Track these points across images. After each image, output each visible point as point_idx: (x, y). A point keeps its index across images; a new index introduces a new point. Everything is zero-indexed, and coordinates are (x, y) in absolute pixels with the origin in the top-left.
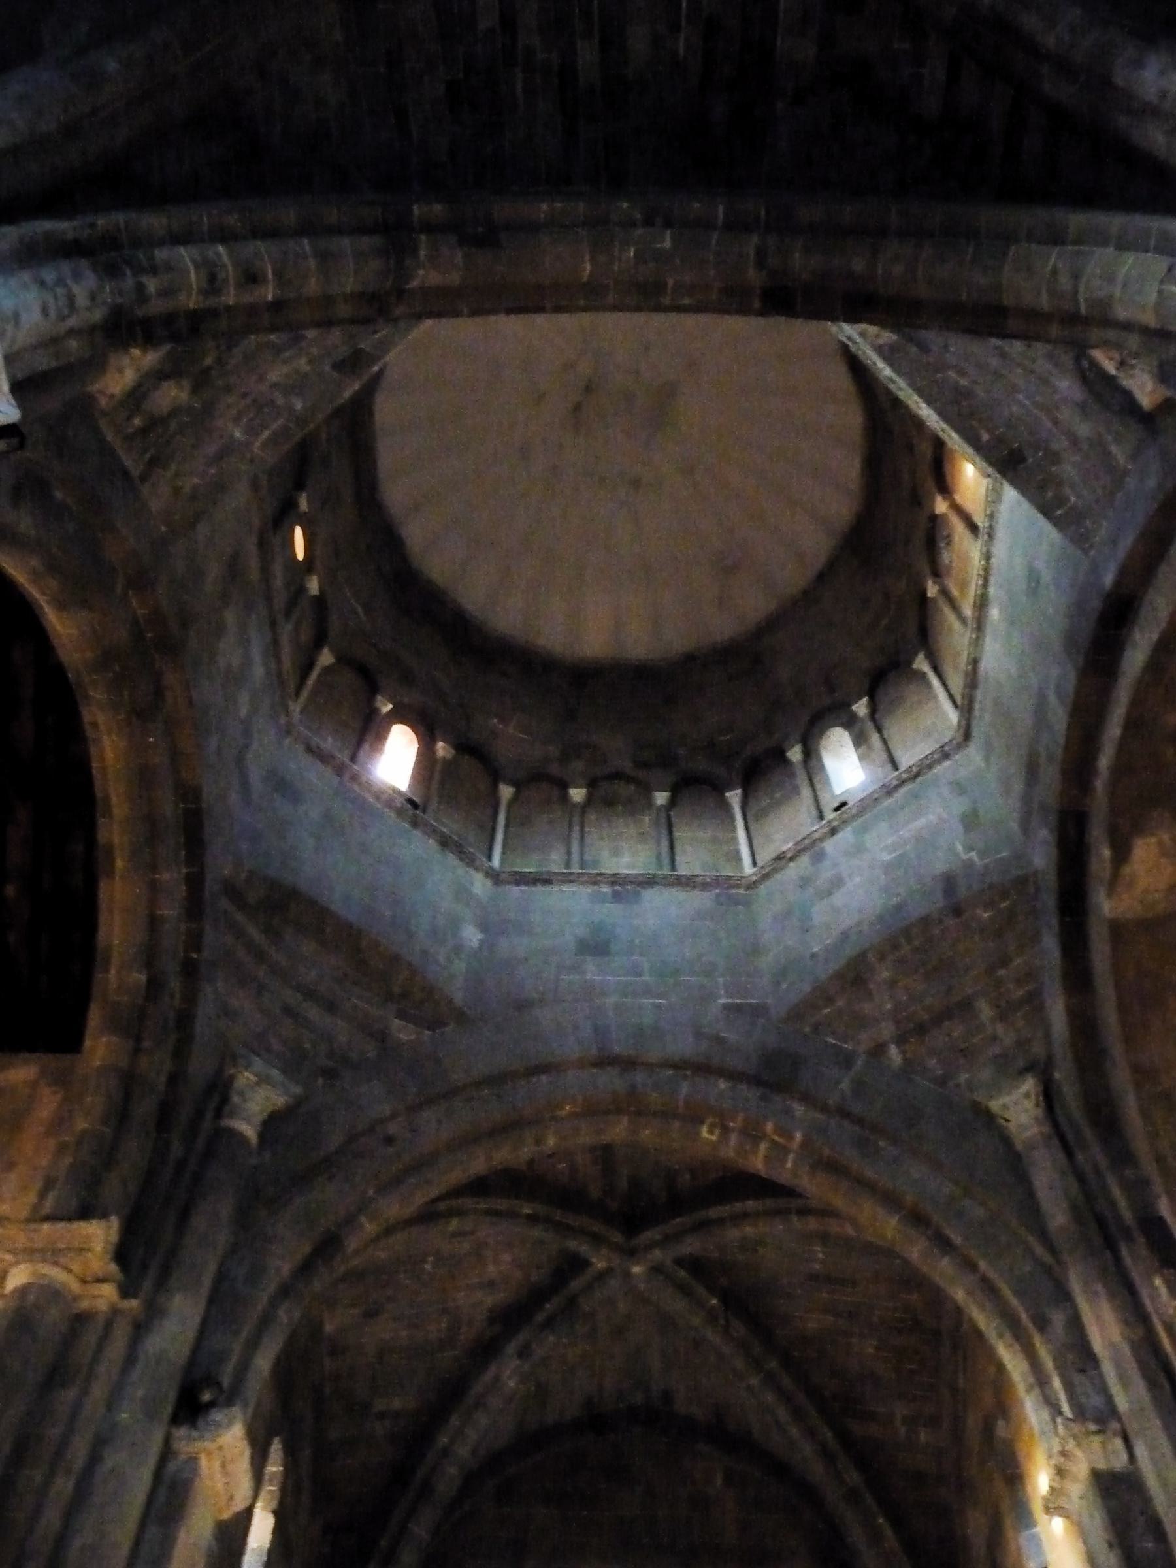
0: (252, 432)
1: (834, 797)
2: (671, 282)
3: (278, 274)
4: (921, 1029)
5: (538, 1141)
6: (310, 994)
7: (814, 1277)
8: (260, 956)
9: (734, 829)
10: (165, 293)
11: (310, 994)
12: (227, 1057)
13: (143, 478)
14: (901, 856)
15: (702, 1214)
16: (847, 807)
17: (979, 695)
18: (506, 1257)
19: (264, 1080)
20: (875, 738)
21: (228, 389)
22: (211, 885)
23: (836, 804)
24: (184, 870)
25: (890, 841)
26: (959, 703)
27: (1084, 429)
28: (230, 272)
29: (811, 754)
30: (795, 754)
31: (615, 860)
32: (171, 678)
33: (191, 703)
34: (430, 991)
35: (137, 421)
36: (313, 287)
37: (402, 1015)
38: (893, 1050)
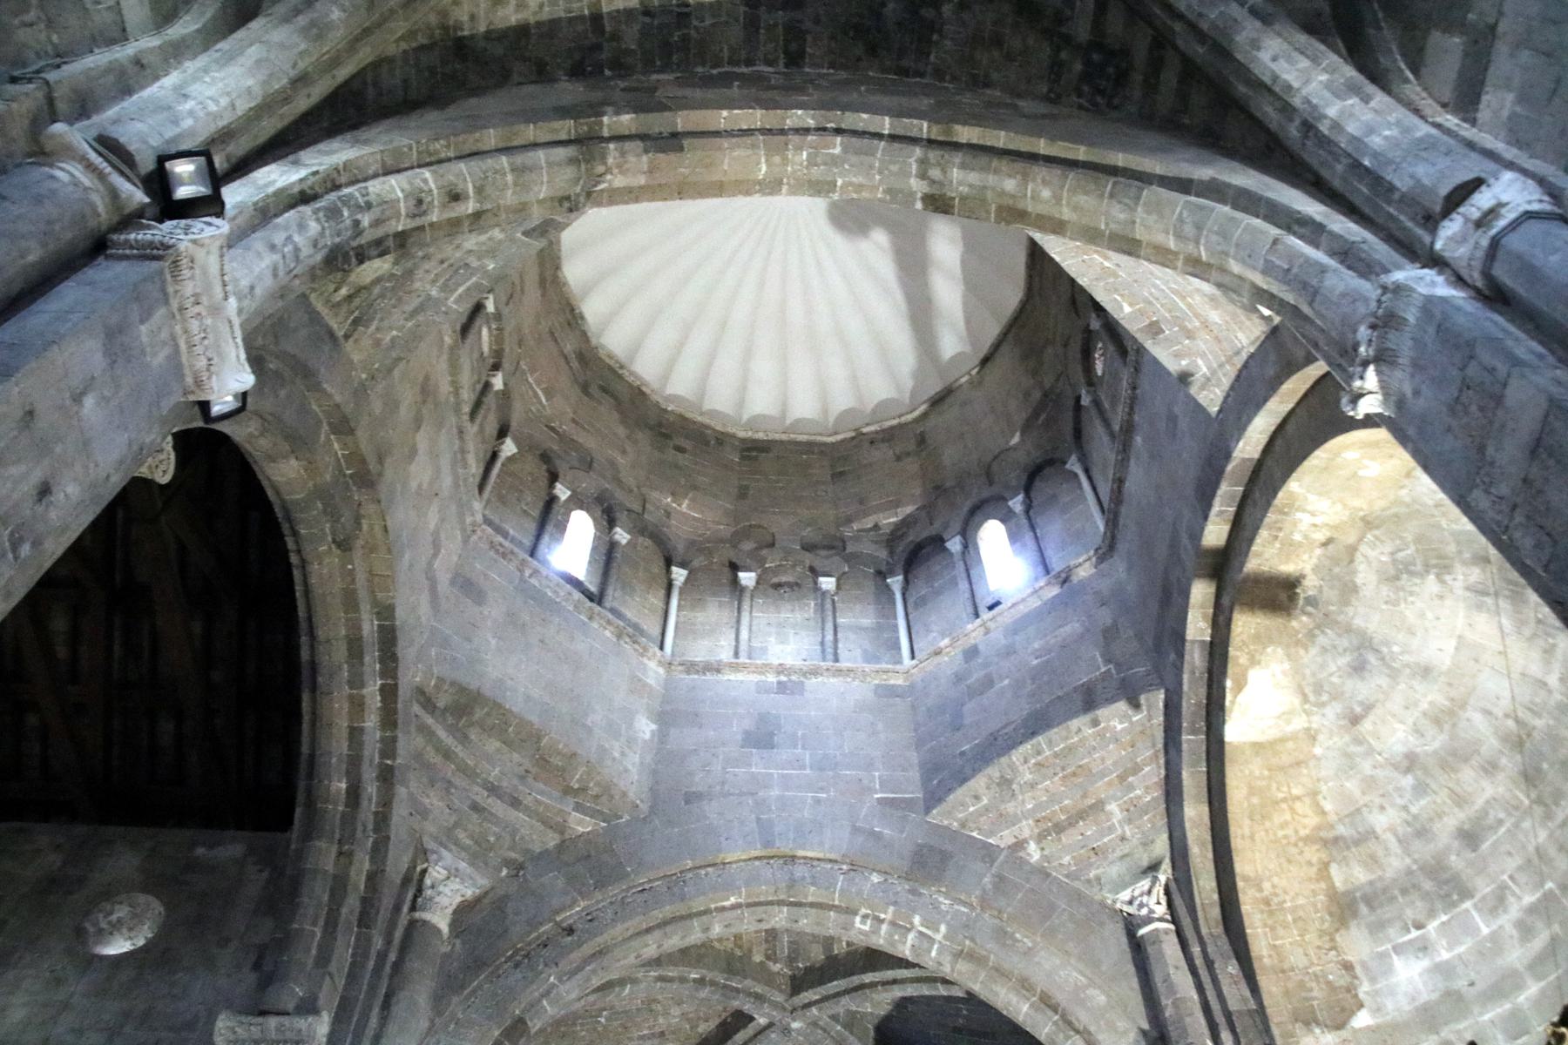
0: (447, 288)
1: (989, 593)
2: (840, 182)
3: (480, 190)
4: (1059, 828)
5: (707, 930)
6: (493, 790)
7: (957, 1030)
8: (448, 755)
9: (895, 617)
10: (376, 223)
11: (493, 790)
12: (422, 853)
13: (347, 337)
14: (1047, 662)
15: (856, 980)
16: (1000, 607)
17: (1123, 510)
18: (675, 1011)
19: (453, 873)
20: (1029, 536)
21: (426, 257)
22: (404, 692)
23: (990, 604)
24: (379, 682)
25: (1036, 645)
26: (1106, 506)
27: (1215, 316)
28: (436, 197)
29: (969, 544)
30: (954, 545)
31: (781, 647)
32: (370, 509)
33: (385, 529)
34: (607, 789)
35: (344, 291)
36: (510, 198)
37: (578, 808)
38: (1032, 847)
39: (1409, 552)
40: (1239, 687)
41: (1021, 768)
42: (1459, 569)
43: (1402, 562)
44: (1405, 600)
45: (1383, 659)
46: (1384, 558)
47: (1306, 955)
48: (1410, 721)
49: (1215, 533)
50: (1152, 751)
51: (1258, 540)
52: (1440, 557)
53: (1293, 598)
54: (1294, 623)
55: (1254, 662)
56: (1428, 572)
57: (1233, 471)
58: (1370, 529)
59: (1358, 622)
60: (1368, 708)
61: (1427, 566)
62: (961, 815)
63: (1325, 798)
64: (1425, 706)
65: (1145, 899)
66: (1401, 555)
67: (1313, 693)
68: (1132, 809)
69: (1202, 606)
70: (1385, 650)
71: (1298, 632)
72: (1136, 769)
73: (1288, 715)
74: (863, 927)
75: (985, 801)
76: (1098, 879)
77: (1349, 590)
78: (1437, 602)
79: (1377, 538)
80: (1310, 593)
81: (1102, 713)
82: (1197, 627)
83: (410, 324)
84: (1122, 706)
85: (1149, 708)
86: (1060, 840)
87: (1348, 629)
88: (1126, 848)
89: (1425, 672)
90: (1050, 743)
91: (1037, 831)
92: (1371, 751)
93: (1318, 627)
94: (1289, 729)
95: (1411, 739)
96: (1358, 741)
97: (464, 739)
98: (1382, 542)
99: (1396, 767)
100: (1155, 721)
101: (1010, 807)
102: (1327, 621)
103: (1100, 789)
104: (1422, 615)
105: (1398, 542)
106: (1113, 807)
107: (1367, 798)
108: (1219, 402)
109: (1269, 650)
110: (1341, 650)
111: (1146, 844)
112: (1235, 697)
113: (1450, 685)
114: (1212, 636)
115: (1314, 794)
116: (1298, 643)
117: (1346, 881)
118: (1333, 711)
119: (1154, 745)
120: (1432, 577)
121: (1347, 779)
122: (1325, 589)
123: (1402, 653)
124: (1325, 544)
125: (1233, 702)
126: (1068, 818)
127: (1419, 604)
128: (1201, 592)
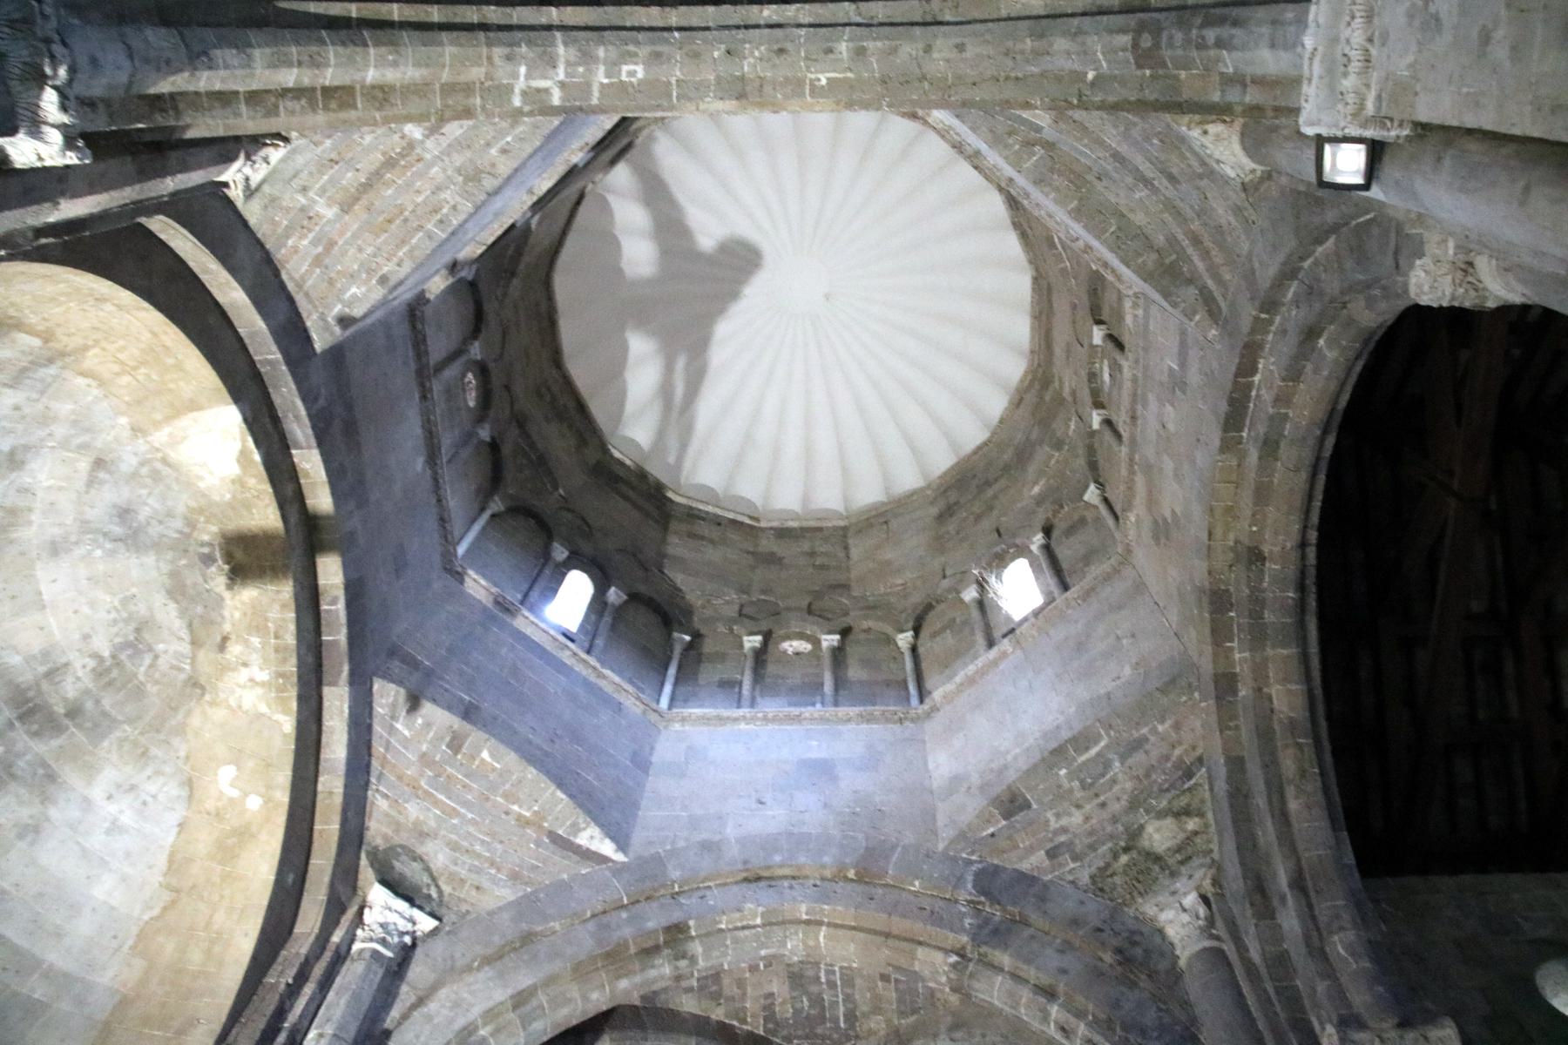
39: (142, 669)
40: (243, 456)
41: (458, 199)
42: (88, 682)
43: (144, 652)
44: (117, 611)
45: (105, 534)
46: (161, 647)
48: (40, 494)
49: (331, 572)
50: (305, 288)
51: (292, 627)
52: (110, 684)
53: (229, 557)
54: (214, 529)
55: (239, 482)
56: (114, 657)
57: (341, 664)
58: (190, 678)
59: (150, 559)
60: (91, 482)
61: (118, 664)
62: (521, 129)
63: (89, 386)
64: (35, 517)
66: (148, 660)
67: (159, 470)
68: (305, 223)
69: (314, 484)
70: (109, 546)
71: (207, 521)
72: (317, 261)
73: (175, 442)
74: (632, 67)
75: (493, 151)
77: (177, 590)
78: (87, 630)
79: (180, 669)
80: (213, 569)
82: (310, 463)
83: (1145, 731)
85: (327, 328)
86: (384, 154)
87: (157, 546)
89: (55, 549)
90: (430, 236)
91: (418, 150)
92: (64, 444)
93: (188, 536)
94: (167, 430)
95: (29, 480)
96: (83, 447)
97: (1172, 241)
98: (172, 667)
99: (27, 448)
100: (315, 316)
102: (181, 545)
104: (92, 604)
105: (157, 675)
106: (329, 213)
107: (40, 406)
108: (376, 697)
109: (228, 496)
110: (154, 522)
112: (244, 446)
113: (22, 554)
114: (290, 456)
116: (201, 511)
117: (13, 341)
118: (128, 462)
119: (307, 295)
120: (106, 654)
121: (73, 411)
122: (200, 580)
123: (89, 553)
124: (225, 639)
125: (244, 441)
126: (382, 177)
127: (102, 615)
128: (321, 499)
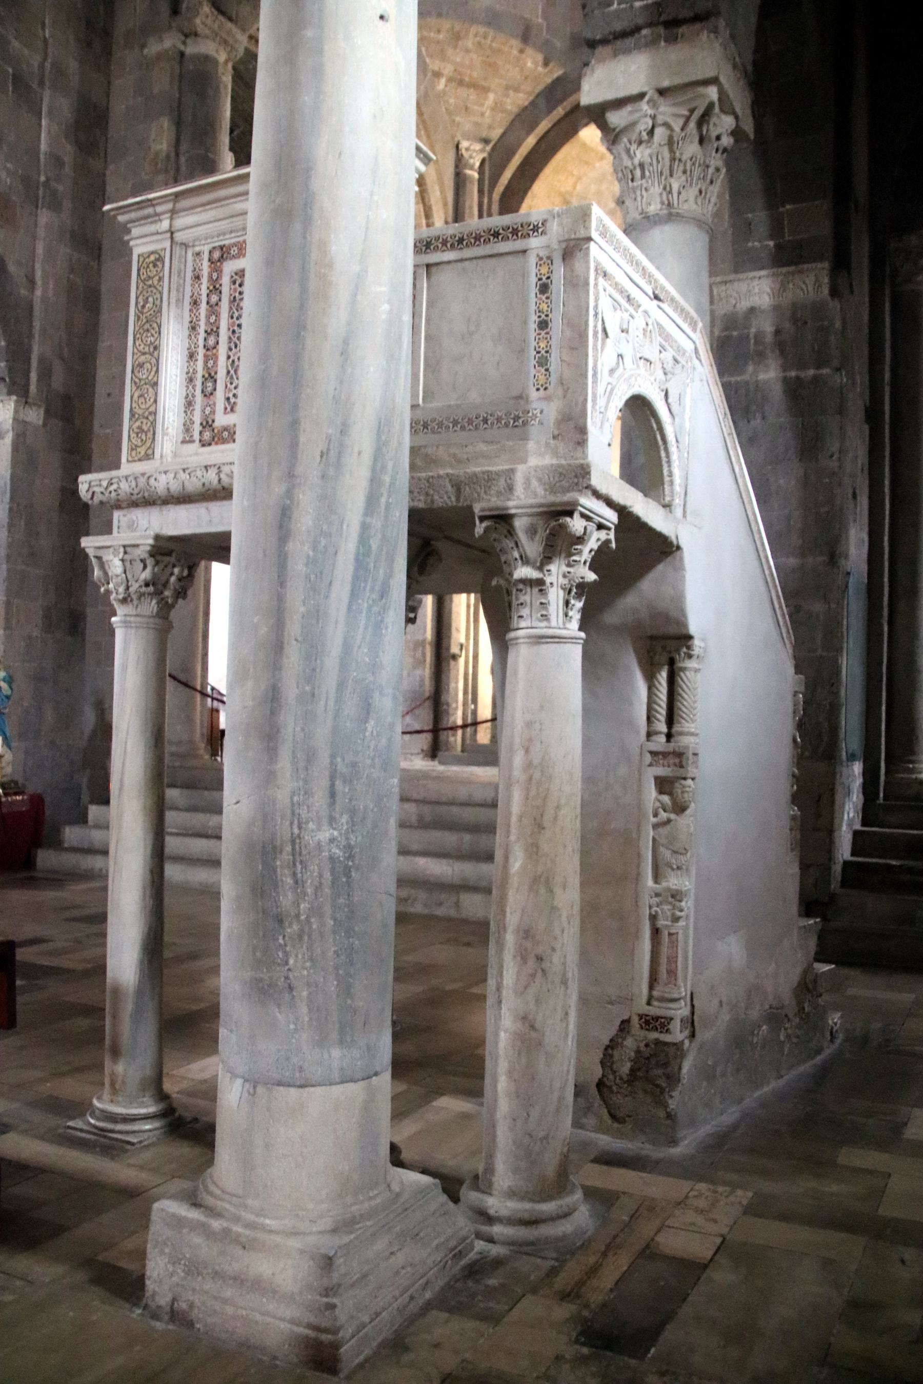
4: (461, 83)
38: (443, 81)
47: (760, 278)
65: (474, 154)
72: (517, 90)
76: (459, 124)
81: (530, 51)
84: (540, 58)
88: (479, 119)
101: (450, 52)
103: (495, 83)
106: (491, 96)
111: (490, 127)
115: (579, 178)
